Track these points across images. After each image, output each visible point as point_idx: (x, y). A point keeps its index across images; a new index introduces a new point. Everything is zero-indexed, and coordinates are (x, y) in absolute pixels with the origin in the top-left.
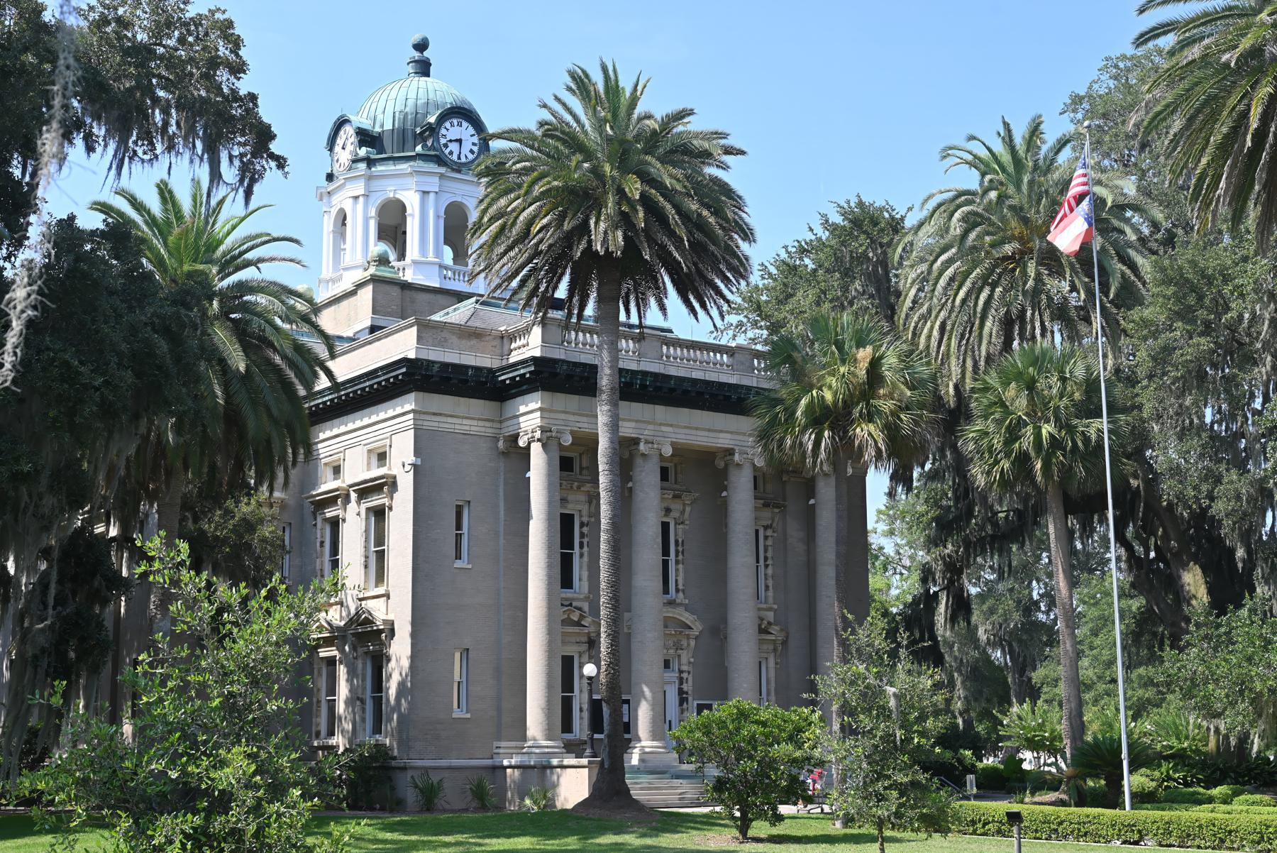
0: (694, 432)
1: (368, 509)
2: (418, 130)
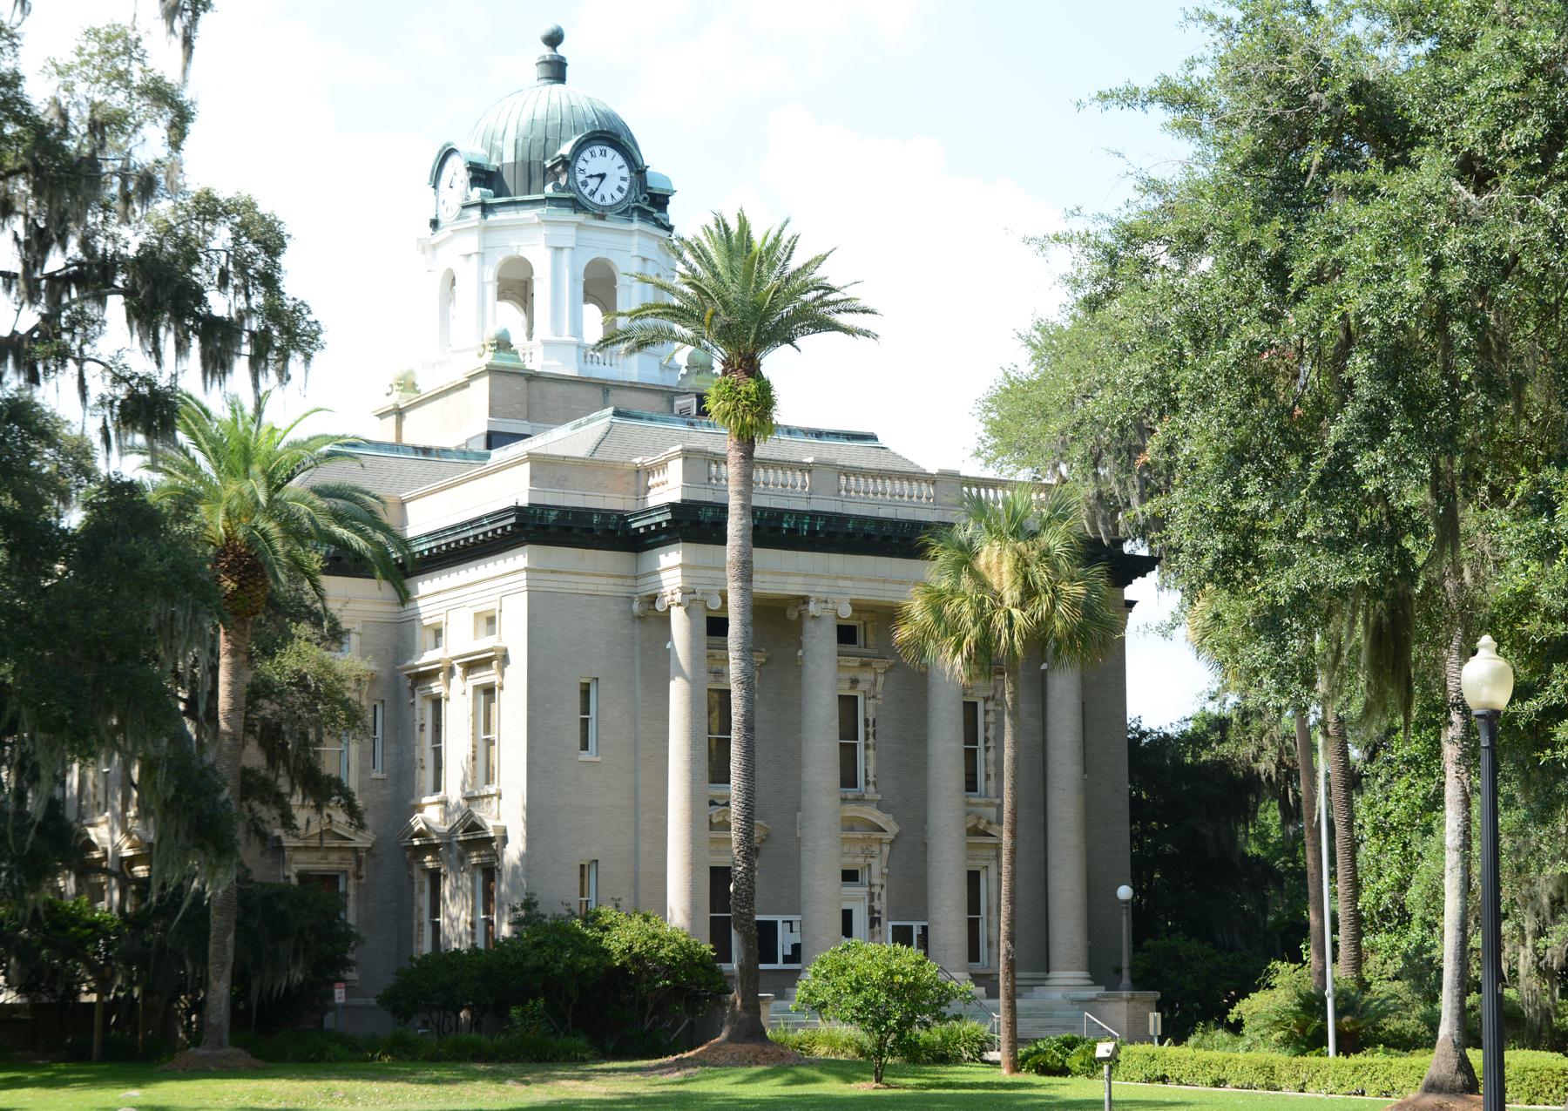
0: (881, 586)
1: (476, 687)
2: (548, 164)
